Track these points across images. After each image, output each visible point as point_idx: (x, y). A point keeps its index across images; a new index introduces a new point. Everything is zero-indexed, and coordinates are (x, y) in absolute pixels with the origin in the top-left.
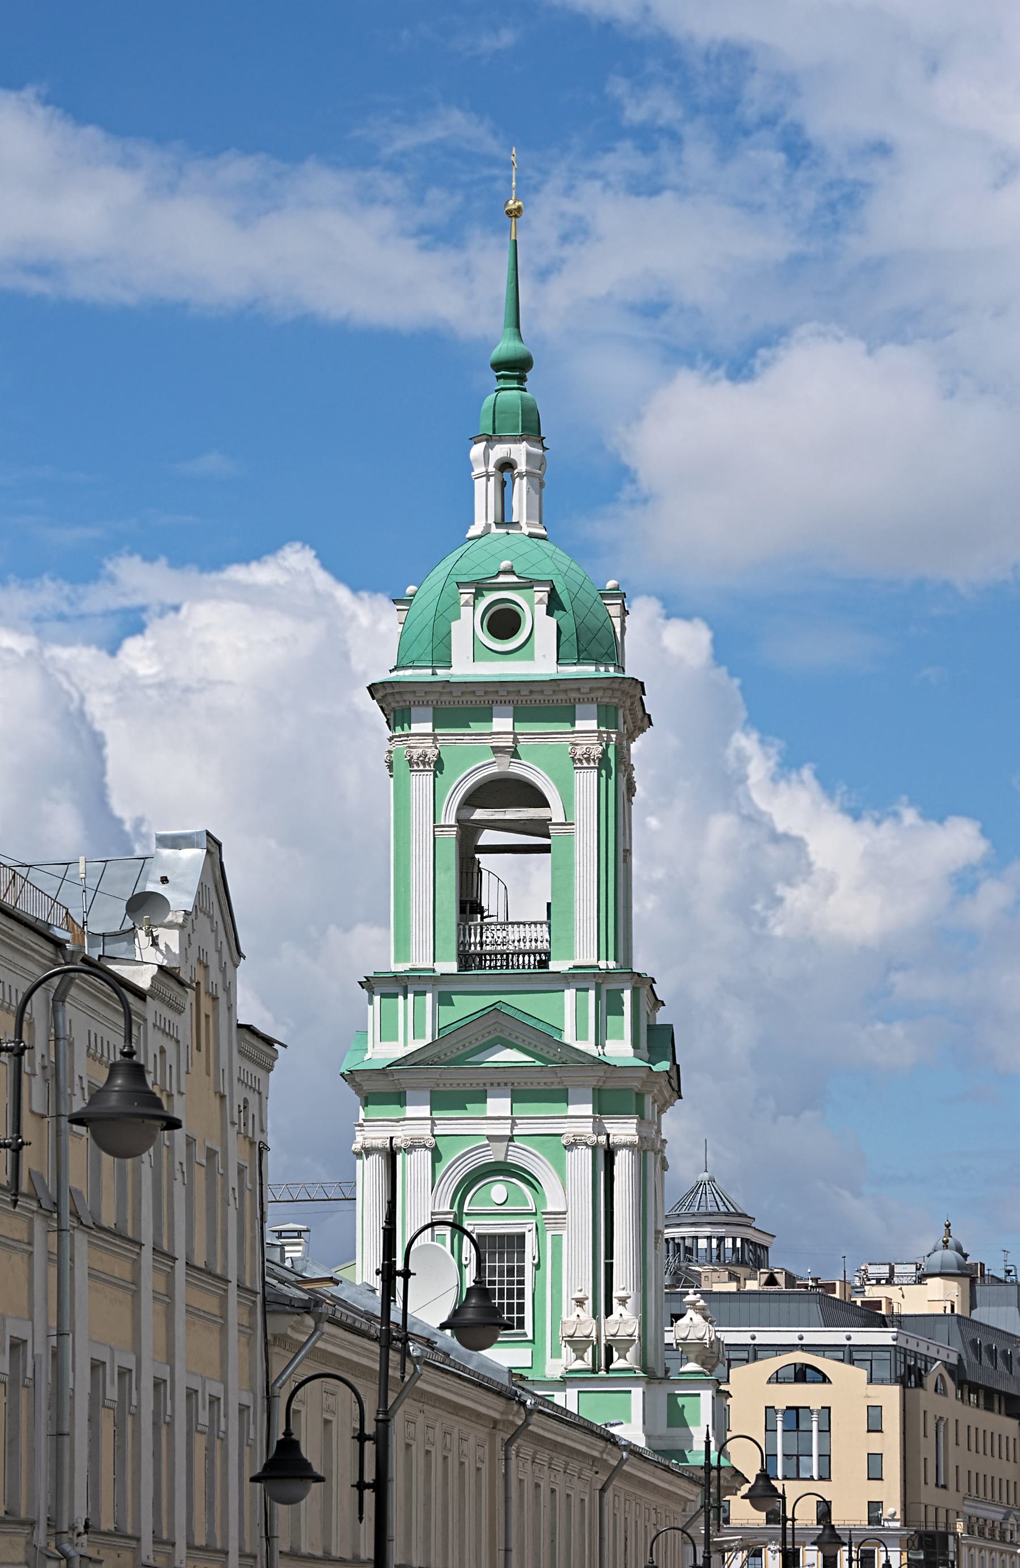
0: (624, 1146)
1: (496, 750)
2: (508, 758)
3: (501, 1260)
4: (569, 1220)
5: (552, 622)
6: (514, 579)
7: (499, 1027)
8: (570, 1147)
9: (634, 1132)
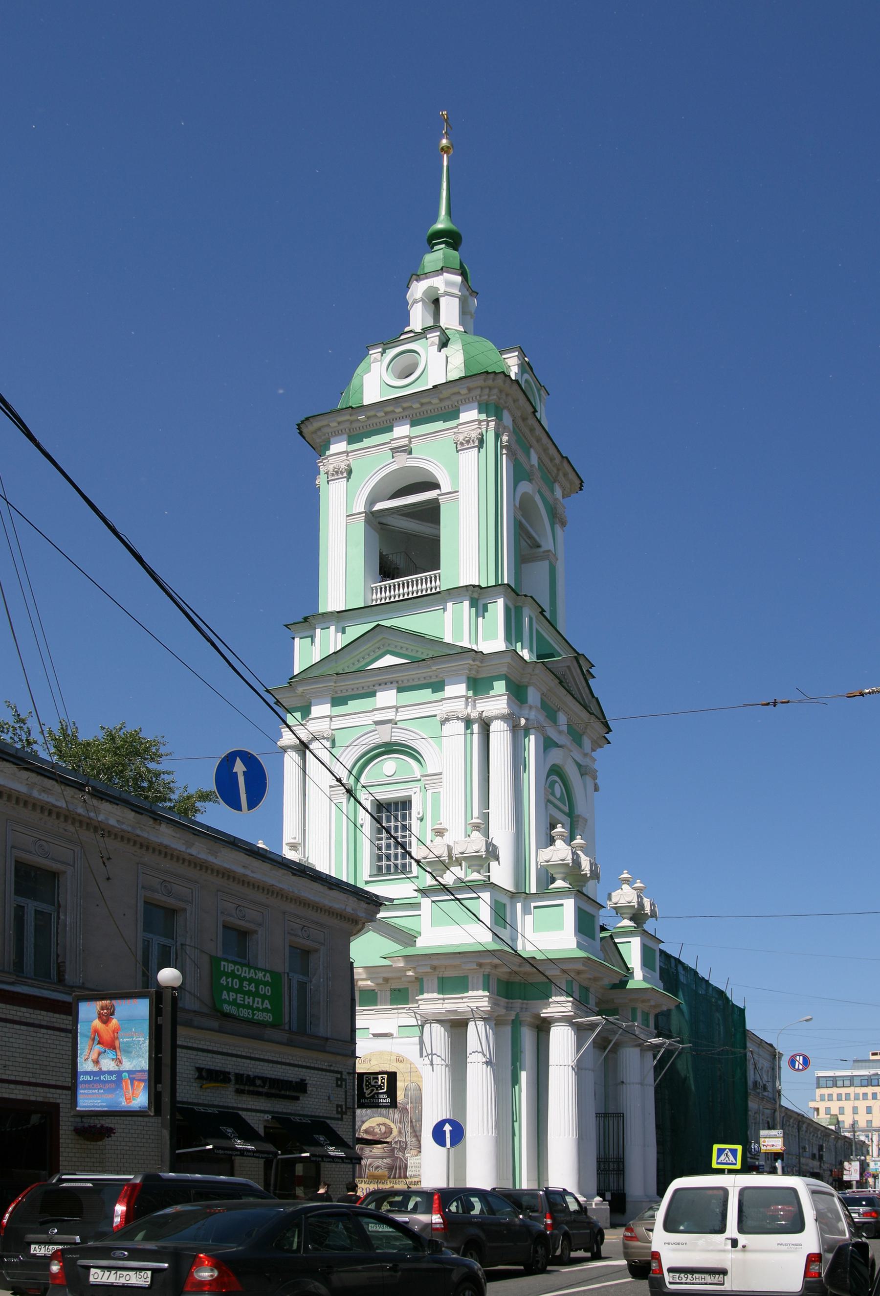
1: (395, 450)
2: (404, 456)
3: (396, 820)
4: (444, 780)
8: (444, 722)
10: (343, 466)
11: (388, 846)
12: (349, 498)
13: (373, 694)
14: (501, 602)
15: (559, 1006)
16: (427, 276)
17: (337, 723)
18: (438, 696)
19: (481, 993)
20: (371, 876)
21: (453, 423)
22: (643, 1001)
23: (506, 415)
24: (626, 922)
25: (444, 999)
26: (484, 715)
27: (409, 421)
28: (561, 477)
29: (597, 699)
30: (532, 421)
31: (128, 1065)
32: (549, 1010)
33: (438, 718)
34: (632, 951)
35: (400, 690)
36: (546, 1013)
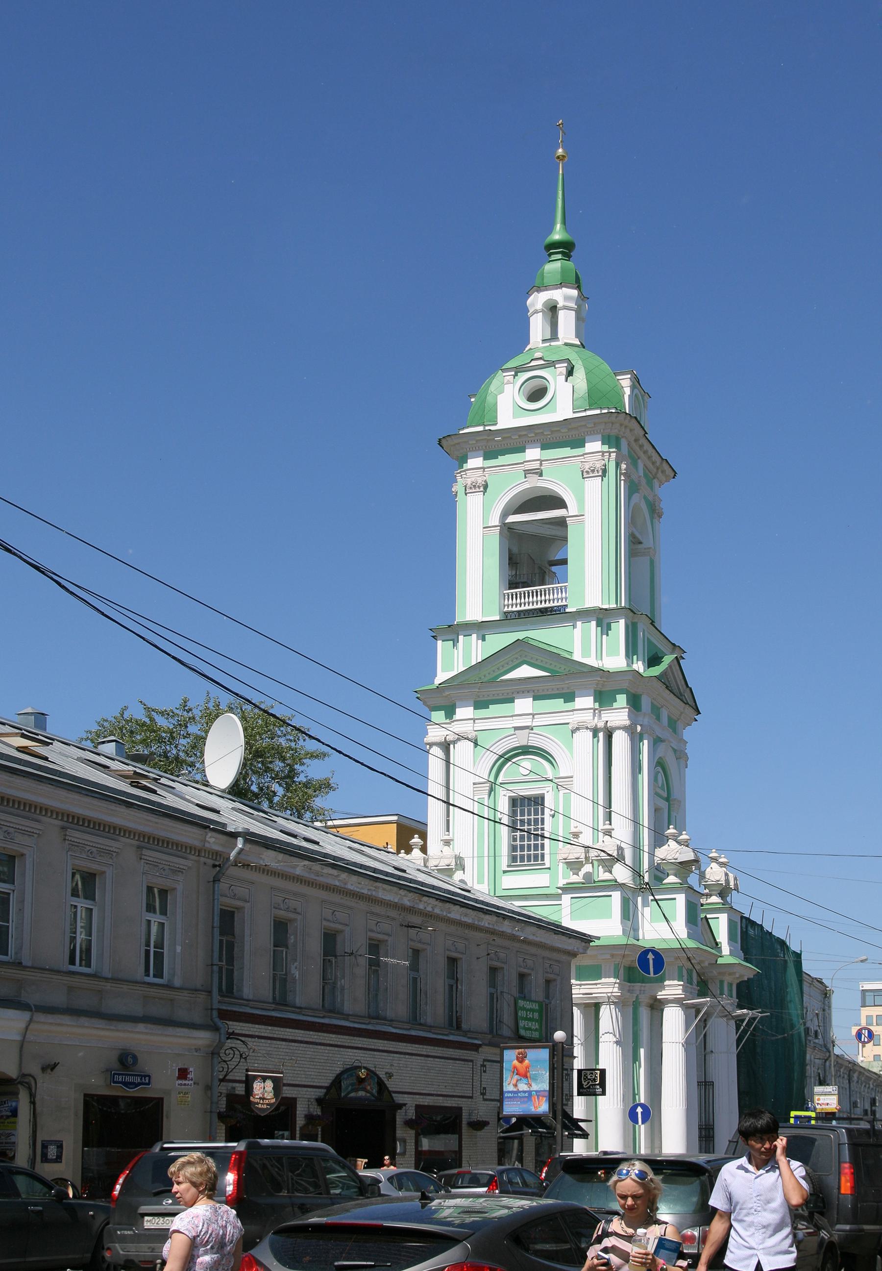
0: (619, 728)
1: (527, 472)
2: (536, 477)
4: (575, 782)
5: (568, 386)
6: (542, 362)
7: (521, 652)
9: (680, 992)
10: (480, 481)
11: (522, 838)
12: (486, 511)
13: (511, 700)
14: (622, 622)
15: (673, 989)
16: (547, 288)
17: (480, 725)
18: (569, 706)
19: (612, 980)
20: (508, 866)
21: (578, 451)
22: (730, 974)
23: (624, 443)
24: (715, 899)
25: (580, 985)
26: (609, 724)
27: (539, 445)
28: (660, 475)
29: (691, 689)
30: (642, 441)
31: (535, 1087)
32: (664, 992)
33: (570, 726)
34: (721, 926)
35: (536, 698)
36: (661, 995)
